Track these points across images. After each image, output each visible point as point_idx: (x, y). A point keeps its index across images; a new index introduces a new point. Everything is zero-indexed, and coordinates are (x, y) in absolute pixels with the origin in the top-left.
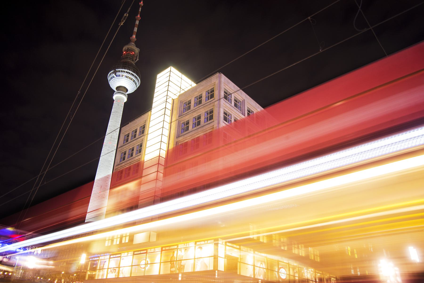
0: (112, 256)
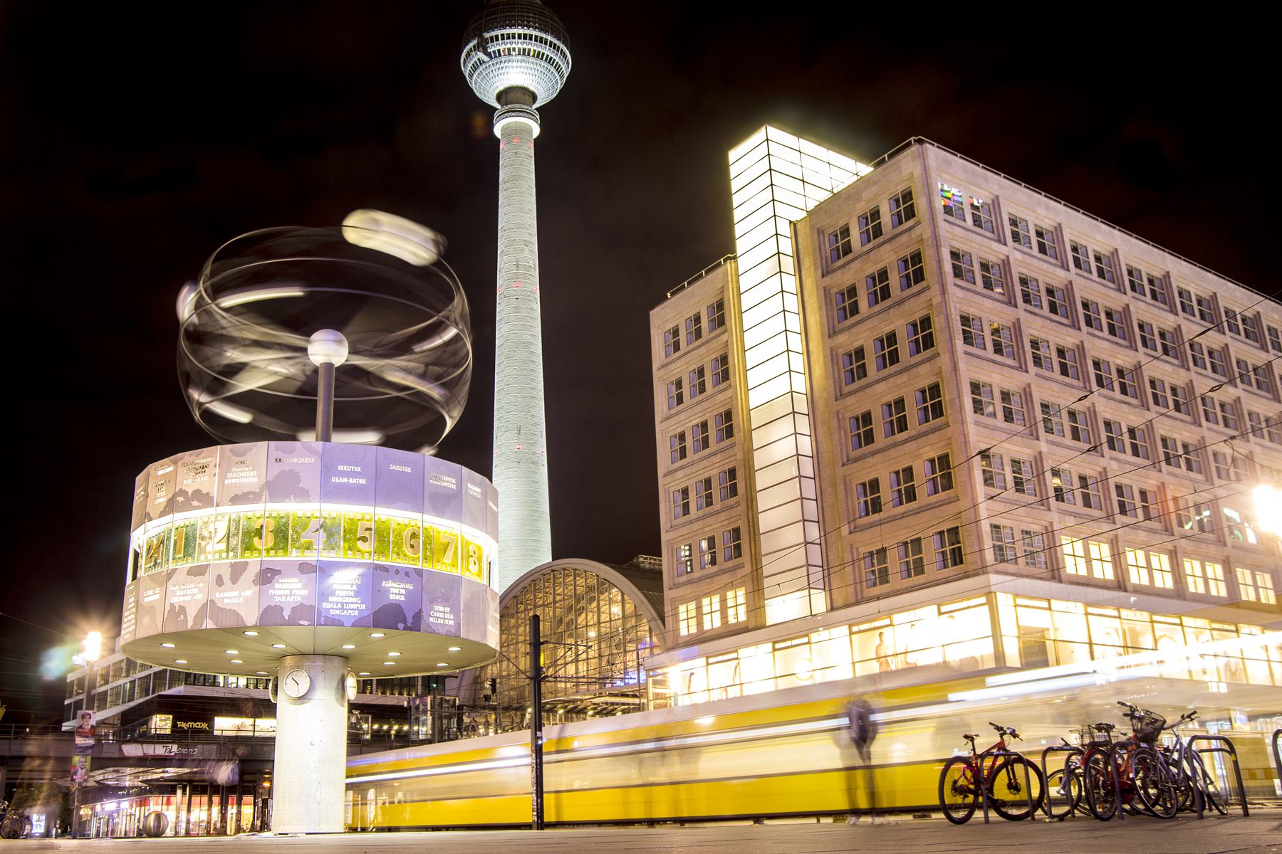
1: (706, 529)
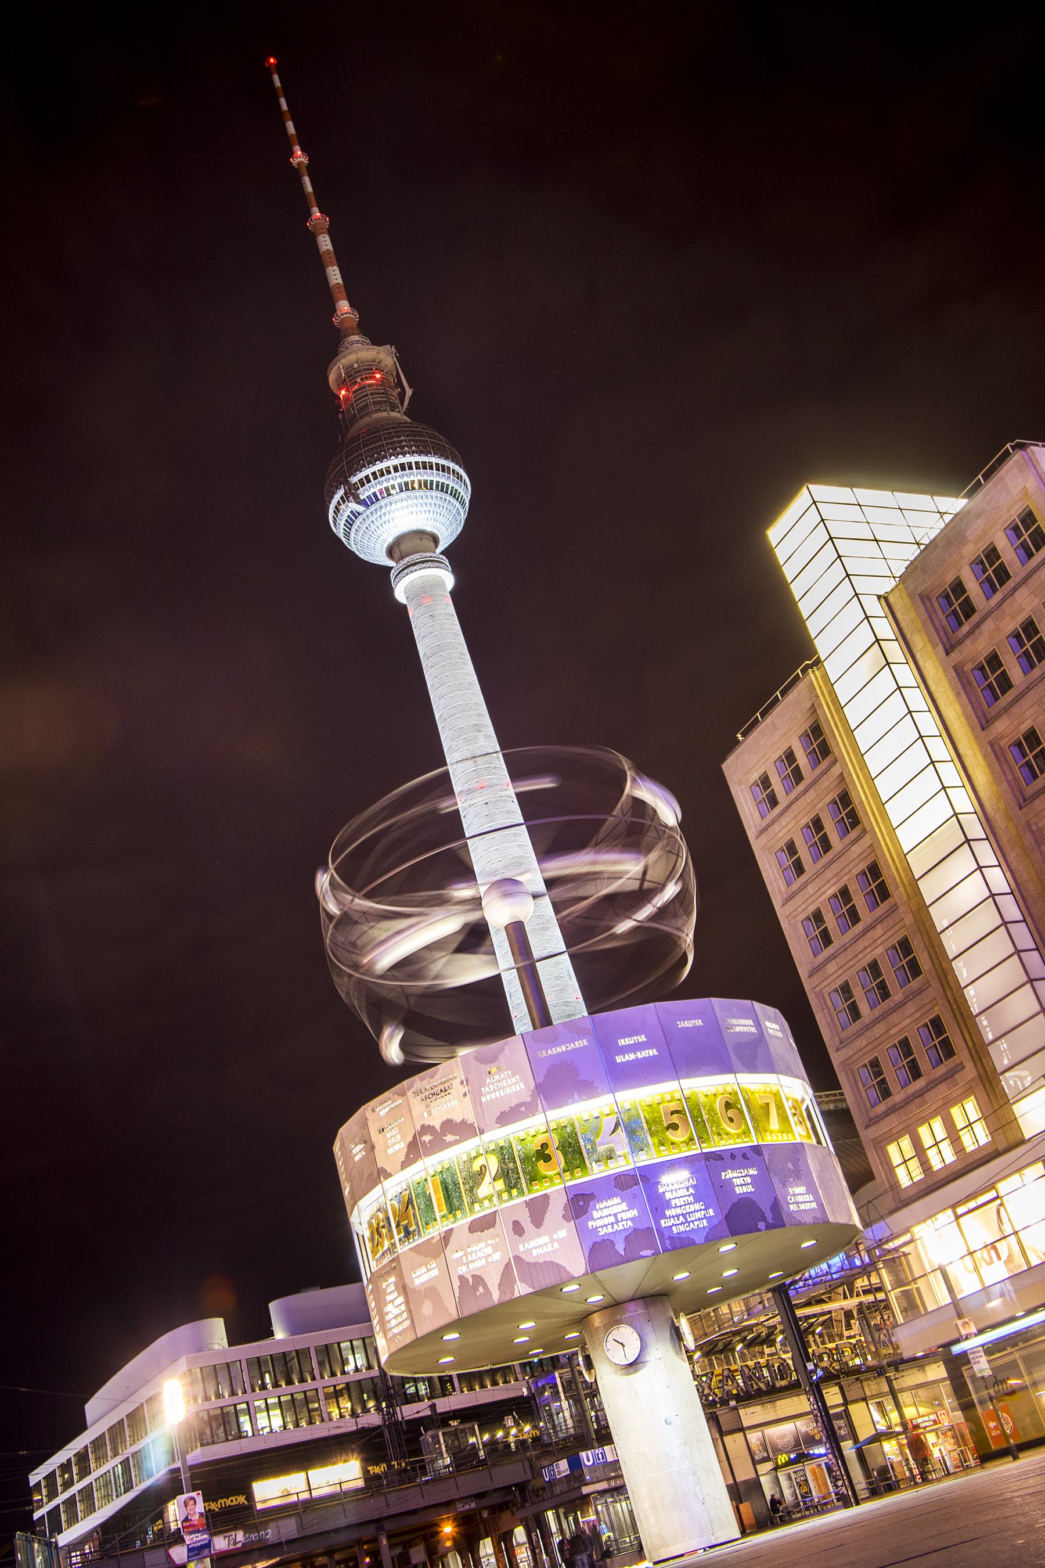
0: (960, 1210)
1: (892, 1032)
